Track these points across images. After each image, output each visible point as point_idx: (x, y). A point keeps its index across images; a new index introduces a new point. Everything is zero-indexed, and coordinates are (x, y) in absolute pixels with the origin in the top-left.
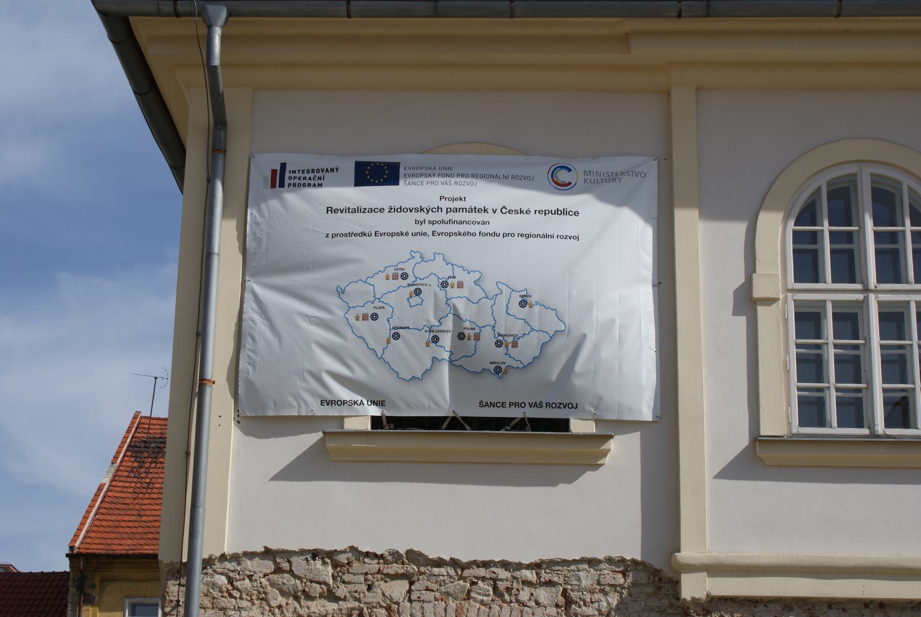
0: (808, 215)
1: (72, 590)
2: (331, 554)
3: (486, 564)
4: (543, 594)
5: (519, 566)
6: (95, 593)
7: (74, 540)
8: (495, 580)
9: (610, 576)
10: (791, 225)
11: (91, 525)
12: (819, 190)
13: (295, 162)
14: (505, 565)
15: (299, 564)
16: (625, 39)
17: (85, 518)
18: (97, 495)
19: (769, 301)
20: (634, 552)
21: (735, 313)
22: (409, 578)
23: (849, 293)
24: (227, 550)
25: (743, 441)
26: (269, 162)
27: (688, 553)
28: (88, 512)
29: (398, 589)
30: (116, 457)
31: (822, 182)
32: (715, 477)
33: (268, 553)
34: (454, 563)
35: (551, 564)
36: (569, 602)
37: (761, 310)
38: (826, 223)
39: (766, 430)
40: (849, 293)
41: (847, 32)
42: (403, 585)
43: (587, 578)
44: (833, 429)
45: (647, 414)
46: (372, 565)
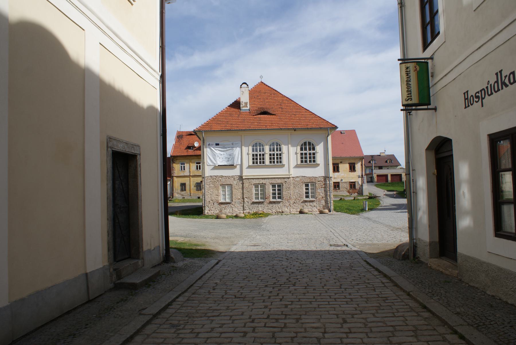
0: (253, 146)
1: (171, 161)
4: (232, 178)
6: (175, 162)
7: (171, 154)
8: (228, 178)
11: (173, 151)
13: (210, 143)
15: (213, 177)
16: (238, 132)
17: (172, 150)
18: (173, 146)
19: (250, 154)
20: (239, 175)
21: (295, 154)
22: (222, 177)
25: (248, 166)
26: (208, 143)
27: (243, 175)
28: (172, 149)
29: (221, 178)
30: (175, 139)
33: (210, 176)
34: (225, 176)
35: (233, 176)
36: (234, 179)
37: (249, 155)
39: (250, 165)
43: (236, 177)
45: (240, 164)
46: (219, 177)
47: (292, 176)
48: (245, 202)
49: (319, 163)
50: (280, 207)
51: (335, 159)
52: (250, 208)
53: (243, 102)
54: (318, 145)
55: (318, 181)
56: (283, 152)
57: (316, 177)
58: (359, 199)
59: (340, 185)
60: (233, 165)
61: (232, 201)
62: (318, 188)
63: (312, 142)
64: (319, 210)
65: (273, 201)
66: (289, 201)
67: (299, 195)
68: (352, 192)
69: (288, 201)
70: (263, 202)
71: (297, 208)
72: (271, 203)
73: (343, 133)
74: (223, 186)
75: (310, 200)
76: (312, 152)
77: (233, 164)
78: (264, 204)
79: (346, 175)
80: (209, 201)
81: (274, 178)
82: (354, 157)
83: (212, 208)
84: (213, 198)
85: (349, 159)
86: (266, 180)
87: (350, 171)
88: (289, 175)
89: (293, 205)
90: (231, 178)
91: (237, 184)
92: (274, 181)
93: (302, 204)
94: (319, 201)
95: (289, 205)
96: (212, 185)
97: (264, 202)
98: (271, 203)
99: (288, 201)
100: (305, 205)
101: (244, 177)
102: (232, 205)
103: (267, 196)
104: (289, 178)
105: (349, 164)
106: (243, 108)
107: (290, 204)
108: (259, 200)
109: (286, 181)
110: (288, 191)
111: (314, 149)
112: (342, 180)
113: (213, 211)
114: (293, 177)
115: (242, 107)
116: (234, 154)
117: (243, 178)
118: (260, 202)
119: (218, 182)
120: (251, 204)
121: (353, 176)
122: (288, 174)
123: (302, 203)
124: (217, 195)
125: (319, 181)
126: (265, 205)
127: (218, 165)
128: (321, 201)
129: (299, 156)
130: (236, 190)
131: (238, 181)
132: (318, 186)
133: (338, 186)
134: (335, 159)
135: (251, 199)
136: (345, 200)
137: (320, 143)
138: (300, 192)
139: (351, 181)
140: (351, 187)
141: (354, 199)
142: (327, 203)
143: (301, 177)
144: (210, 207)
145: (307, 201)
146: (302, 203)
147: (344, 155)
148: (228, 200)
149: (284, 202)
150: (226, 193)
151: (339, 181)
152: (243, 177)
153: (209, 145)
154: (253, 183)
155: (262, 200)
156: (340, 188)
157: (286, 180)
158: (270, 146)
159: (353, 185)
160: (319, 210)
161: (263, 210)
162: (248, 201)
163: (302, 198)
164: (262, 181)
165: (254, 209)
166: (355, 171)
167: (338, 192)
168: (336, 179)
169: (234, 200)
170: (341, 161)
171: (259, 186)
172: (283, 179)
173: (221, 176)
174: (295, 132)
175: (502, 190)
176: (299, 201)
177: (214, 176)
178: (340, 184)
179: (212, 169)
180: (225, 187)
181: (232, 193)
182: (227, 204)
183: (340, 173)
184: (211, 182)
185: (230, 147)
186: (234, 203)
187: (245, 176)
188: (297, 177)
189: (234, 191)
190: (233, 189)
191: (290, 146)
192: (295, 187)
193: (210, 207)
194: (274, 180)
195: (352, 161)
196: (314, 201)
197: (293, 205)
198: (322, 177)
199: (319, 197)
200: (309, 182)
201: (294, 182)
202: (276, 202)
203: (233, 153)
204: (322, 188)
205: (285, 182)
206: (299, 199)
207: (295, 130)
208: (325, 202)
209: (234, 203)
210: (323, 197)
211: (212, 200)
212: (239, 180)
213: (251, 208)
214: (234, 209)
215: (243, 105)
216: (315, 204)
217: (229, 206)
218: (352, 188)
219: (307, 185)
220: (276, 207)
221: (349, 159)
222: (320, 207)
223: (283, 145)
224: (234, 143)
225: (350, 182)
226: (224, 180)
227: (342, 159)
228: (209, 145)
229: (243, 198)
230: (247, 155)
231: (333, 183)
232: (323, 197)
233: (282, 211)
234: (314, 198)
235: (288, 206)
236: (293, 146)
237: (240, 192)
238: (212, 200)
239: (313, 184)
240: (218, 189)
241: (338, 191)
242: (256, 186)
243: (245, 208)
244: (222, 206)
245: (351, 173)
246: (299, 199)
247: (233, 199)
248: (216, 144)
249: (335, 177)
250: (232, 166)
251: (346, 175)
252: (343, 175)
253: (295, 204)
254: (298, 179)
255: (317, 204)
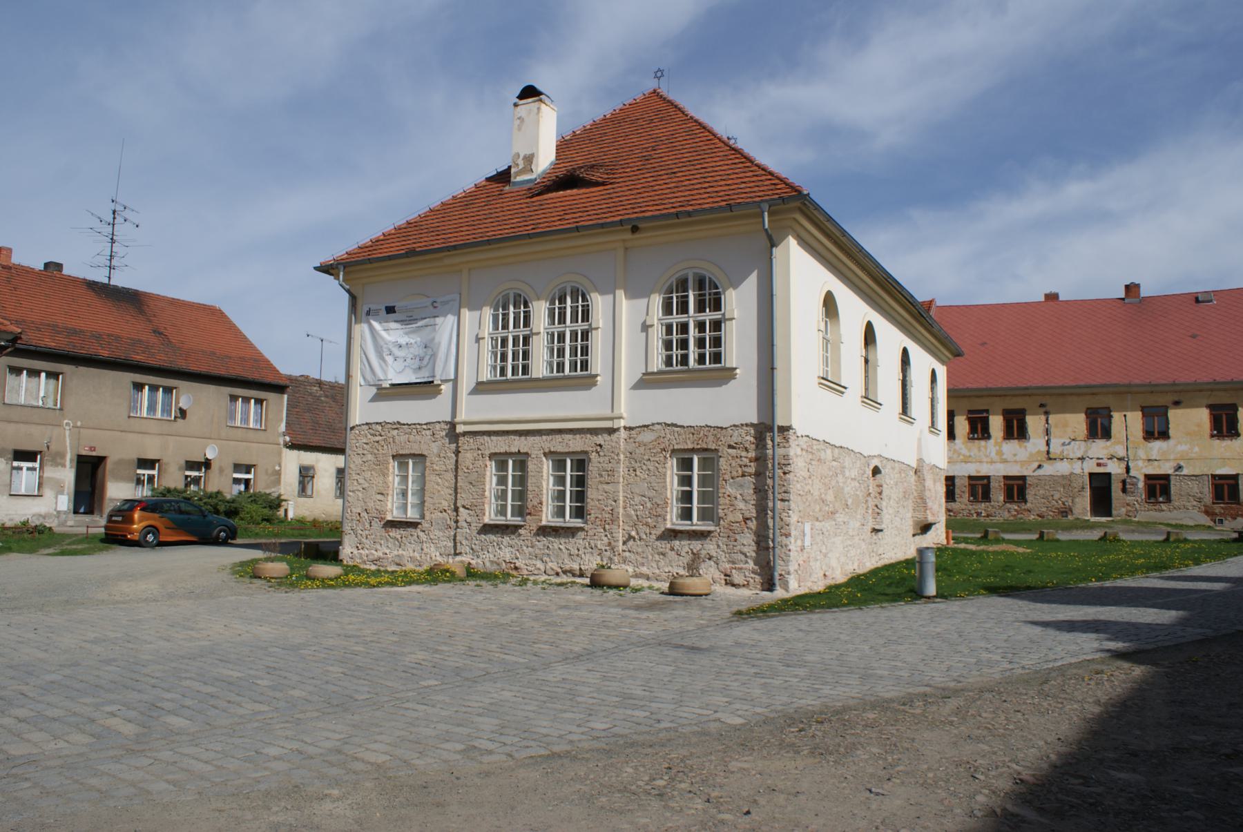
2: (380, 423)
3: (415, 424)
4: (428, 432)
5: (422, 425)
9: (444, 426)
10: (548, 305)
12: (672, 282)
14: (419, 424)
21: (642, 331)
23: (682, 318)
24: (358, 423)
26: (366, 309)
27: (458, 419)
31: (674, 279)
32: (631, 389)
33: (367, 424)
34: (407, 424)
35: (429, 423)
38: (501, 310)
40: (682, 318)
41: (583, 235)
42: (396, 431)
44: (675, 368)
46: (390, 426)
47: (622, 423)
48: (459, 524)
49: (734, 366)
50: (575, 552)
51: (1152, 392)
52: (473, 546)
53: (519, 156)
54: (735, 286)
55: (730, 447)
56: (593, 326)
57: (722, 428)
58: (1058, 541)
59: (1172, 486)
60: (433, 382)
61: (424, 518)
62: (727, 477)
63: (708, 275)
64: (726, 575)
65: (551, 527)
66: (607, 527)
67: (649, 505)
68: (1221, 514)
69: (604, 529)
70: (517, 527)
71: (639, 559)
72: (544, 531)
73: (1203, 302)
74: (401, 458)
75: (694, 531)
76: (708, 316)
77: (431, 380)
78: (520, 535)
79: (1196, 449)
80: (359, 514)
81: (560, 431)
82: (1232, 382)
83: (364, 540)
84: (371, 505)
85: (1212, 390)
86: (531, 439)
87: (1212, 436)
88: (612, 419)
89: (625, 548)
90: (424, 432)
91: (442, 455)
92: (558, 444)
93: (658, 543)
94: (731, 534)
95: (610, 544)
96: (370, 457)
97: (521, 527)
98: (544, 531)
99: (604, 529)
100: (672, 549)
101: (460, 429)
102: (421, 534)
103: (530, 505)
104: (611, 431)
105: (1211, 407)
106: (519, 179)
107: (613, 543)
108: (565, 522)
109: (602, 443)
110: (605, 487)
111: (717, 305)
112: (1179, 468)
113: (367, 552)
114: (631, 429)
115: (515, 173)
116: (436, 340)
117: (458, 431)
118: (507, 527)
119: (385, 447)
120: (480, 533)
121: (1228, 455)
122: (608, 413)
123: (660, 538)
124: (382, 494)
125: (733, 448)
126: (522, 538)
127: (393, 385)
128: (738, 537)
129: (657, 335)
130: (437, 477)
131: (443, 441)
132: (729, 468)
133: (1166, 491)
134: (1152, 392)
135: (479, 512)
136: (1119, 541)
137: (749, 275)
138: (652, 494)
139: (1219, 472)
140: (1218, 494)
141: (1167, 540)
142: (763, 544)
143: (659, 427)
144: (359, 537)
145: (681, 532)
146: (660, 538)
147: (1185, 378)
148: (412, 514)
149: (591, 533)
150: (407, 487)
151: (1170, 472)
152: (458, 426)
153: (368, 313)
154: (487, 453)
155: (517, 520)
156: (1173, 497)
157: (600, 439)
158: (552, 303)
159: (1226, 487)
160: (726, 575)
161: (517, 558)
162: (469, 520)
163: (660, 519)
164: (518, 444)
165: (488, 552)
166: (1237, 435)
167: (1163, 511)
168: (1156, 463)
169: (427, 517)
170: (1176, 399)
171: (510, 462)
172: (591, 434)
173: (395, 423)
174: (637, 235)
175: (863, 575)
176: (648, 531)
177: (377, 423)
178: (1172, 482)
179: (374, 399)
180: (408, 463)
181: (422, 492)
182: (409, 527)
183: (1171, 442)
184: (367, 444)
185: (425, 318)
186: (427, 525)
187: (465, 423)
188: (645, 426)
189: (431, 478)
190: (427, 472)
191: (620, 294)
192: (635, 471)
193: (359, 537)
194: (558, 438)
195: (1225, 399)
196: (710, 532)
197: (625, 548)
198: (747, 425)
199: (731, 517)
200: (693, 450)
201: (631, 447)
202: (563, 528)
203: (433, 339)
204: (743, 476)
205: (598, 448)
206: (647, 524)
207: (635, 229)
208: (758, 543)
209: (427, 525)
210: (746, 519)
211: (366, 510)
212: (447, 440)
213: (476, 548)
214: (425, 549)
215: (520, 167)
216: (710, 547)
217: (411, 535)
218: (1222, 499)
219: (686, 464)
220: (560, 549)
221: (1212, 390)
222: (734, 563)
223: (597, 294)
224: (439, 300)
225: (1214, 476)
226: (403, 438)
227: (1180, 392)
228: (368, 313)
229: (456, 510)
230: (476, 342)
231: (1142, 478)
232: (746, 519)
233: (580, 569)
234: (713, 521)
235: (603, 548)
236: (632, 294)
237: (446, 484)
238: (366, 510)
239: (710, 459)
240: (385, 471)
241: (1164, 507)
242: (500, 460)
243: (458, 544)
244: (391, 534)
245: (1217, 442)
246: (647, 524)
247: (426, 509)
248: (387, 308)
249: (1153, 458)
250: (425, 389)
251: (1196, 449)
252: (1183, 448)
253: (631, 543)
254: (647, 437)
255: (718, 546)
